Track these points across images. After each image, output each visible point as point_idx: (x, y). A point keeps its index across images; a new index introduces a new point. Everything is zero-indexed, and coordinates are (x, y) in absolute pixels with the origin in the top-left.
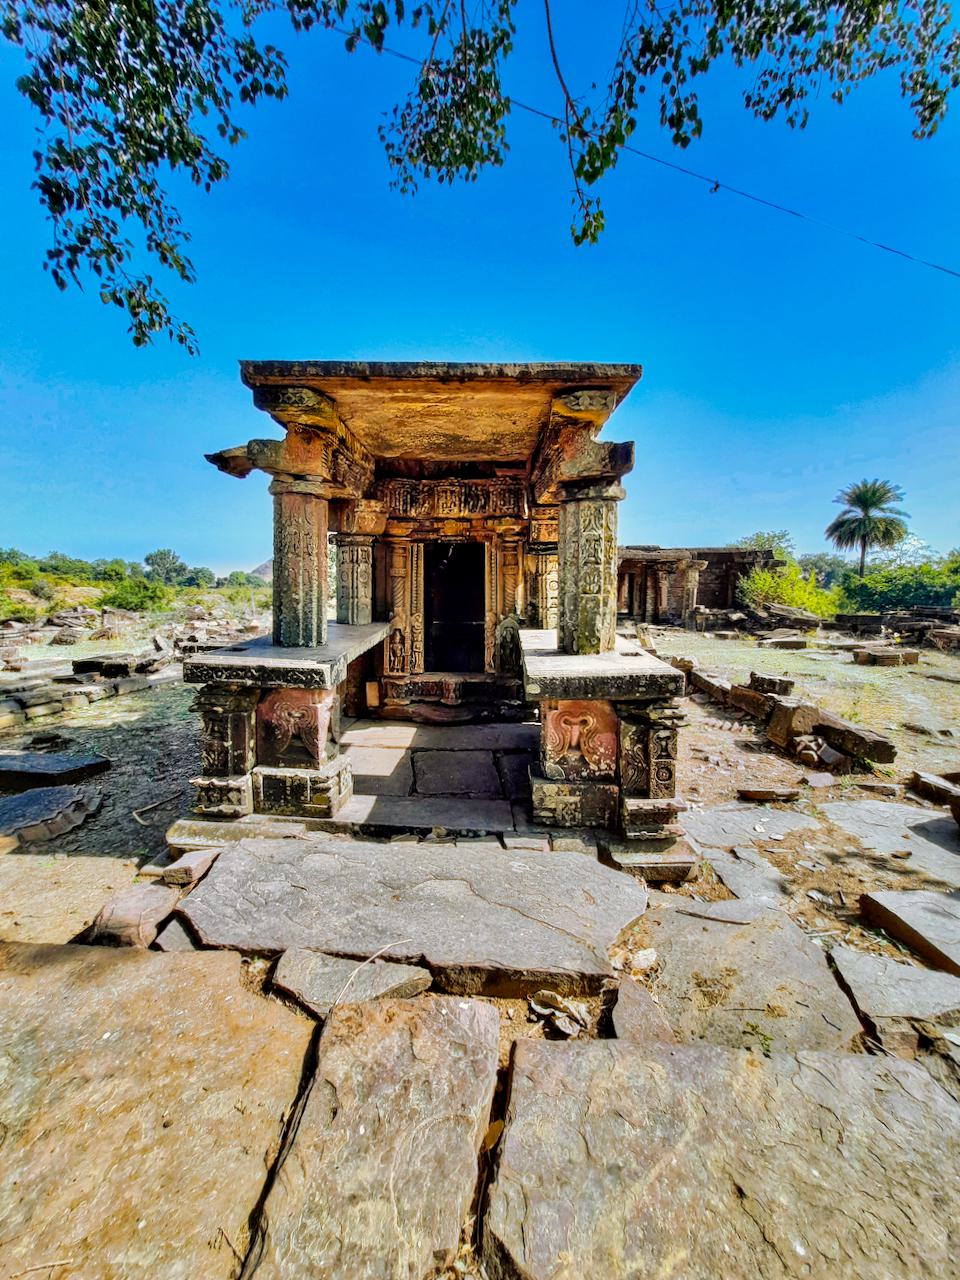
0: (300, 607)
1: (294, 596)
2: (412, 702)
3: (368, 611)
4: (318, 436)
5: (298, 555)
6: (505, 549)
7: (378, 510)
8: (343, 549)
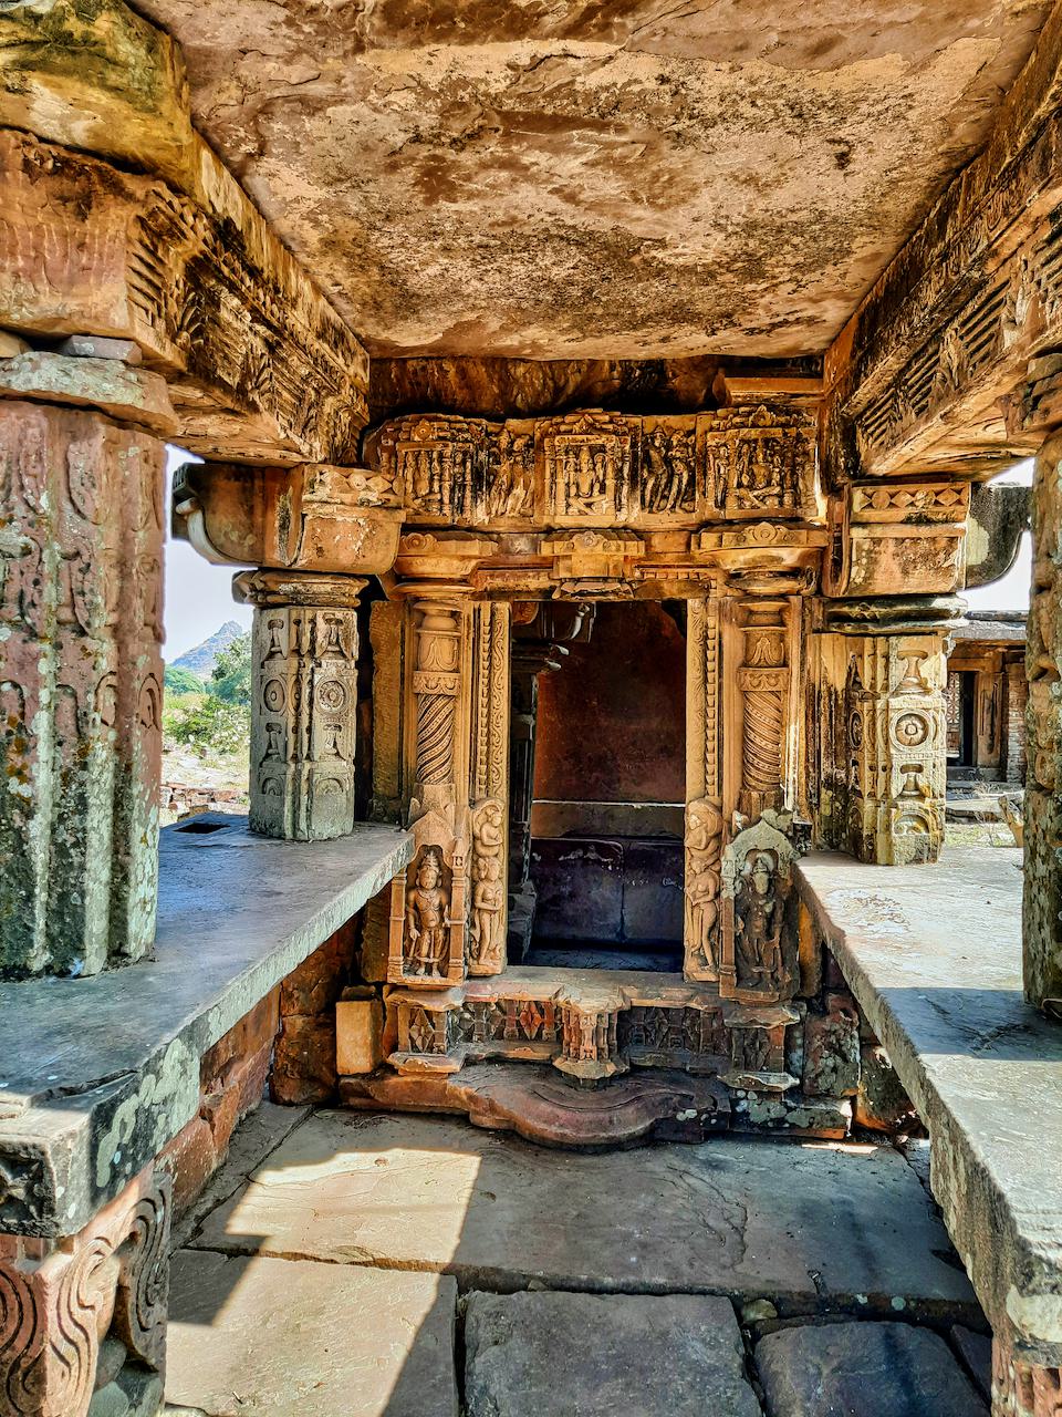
0: (38, 828)
1: (15, 786)
2: (469, 1062)
3: (344, 799)
4: (118, 190)
5: (33, 634)
6: (747, 620)
7: (374, 497)
8: (271, 615)
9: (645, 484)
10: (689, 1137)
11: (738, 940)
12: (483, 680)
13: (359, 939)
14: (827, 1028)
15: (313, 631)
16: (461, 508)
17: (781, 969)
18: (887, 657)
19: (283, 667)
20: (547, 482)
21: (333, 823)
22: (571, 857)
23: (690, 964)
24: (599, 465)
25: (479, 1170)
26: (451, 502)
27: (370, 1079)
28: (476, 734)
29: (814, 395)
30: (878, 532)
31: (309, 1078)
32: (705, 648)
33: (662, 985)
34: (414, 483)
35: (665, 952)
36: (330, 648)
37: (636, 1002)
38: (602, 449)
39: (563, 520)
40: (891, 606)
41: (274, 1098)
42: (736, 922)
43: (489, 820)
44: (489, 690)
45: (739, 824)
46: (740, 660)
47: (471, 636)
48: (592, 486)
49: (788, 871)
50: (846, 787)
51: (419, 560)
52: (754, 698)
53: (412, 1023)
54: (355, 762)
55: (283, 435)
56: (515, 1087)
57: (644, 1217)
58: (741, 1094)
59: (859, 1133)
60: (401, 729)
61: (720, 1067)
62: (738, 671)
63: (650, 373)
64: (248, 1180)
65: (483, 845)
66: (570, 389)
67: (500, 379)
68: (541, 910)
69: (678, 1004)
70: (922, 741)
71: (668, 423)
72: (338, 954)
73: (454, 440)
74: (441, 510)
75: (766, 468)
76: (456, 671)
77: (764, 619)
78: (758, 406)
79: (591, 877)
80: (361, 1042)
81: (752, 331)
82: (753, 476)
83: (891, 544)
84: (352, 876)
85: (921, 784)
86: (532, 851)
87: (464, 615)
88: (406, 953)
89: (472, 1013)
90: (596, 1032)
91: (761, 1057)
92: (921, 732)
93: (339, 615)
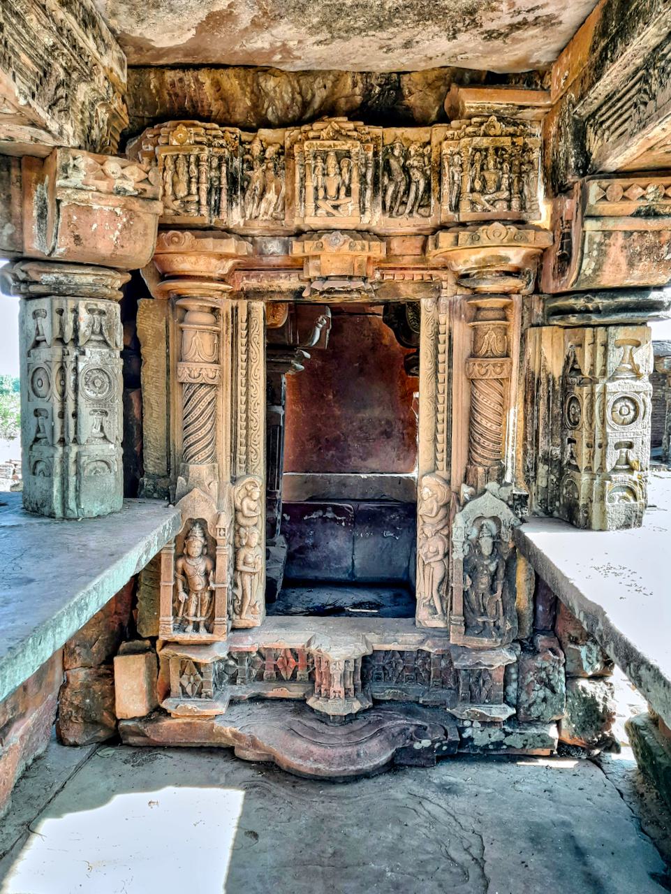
2: (233, 702)
3: (114, 480)
7: (130, 186)
9: (385, 191)
10: (423, 762)
11: (466, 594)
12: (242, 340)
13: (134, 601)
14: (539, 666)
15: (76, 321)
16: (217, 209)
17: (502, 618)
18: (605, 345)
19: (48, 354)
20: (297, 185)
21: (102, 502)
22: (314, 516)
23: (422, 613)
24: (345, 170)
25: (244, 806)
26: (209, 203)
27: (146, 722)
29: (538, 107)
30: (610, 225)
31: (91, 722)
32: (437, 341)
33: (398, 631)
34: (173, 185)
35: (397, 594)
36: (93, 337)
37: (377, 647)
38: (348, 155)
39: (313, 221)
40: (613, 298)
41: (61, 740)
42: (464, 579)
43: (248, 495)
44: (247, 440)
45: (466, 496)
46: (468, 351)
47: (230, 331)
48: (338, 190)
49: (510, 535)
50: (561, 462)
51: (179, 258)
52: (481, 385)
53: (182, 673)
54: (123, 444)
55: (22, 102)
56: (273, 724)
57: (394, 852)
58: (467, 723)
59: (564, 750)
60: (168, 415)
61: (448, 699)
62: (467, 362)
63: (389, 90)
64: (28, 829)
65: (244, 516)
66: (316, 105)
67: (252, 92)
68: (290, 557)
69: (413, 648)
70: (633, 421)
71: (406, 135)
72: (116, 613)
73: (210, 145)
74: (199, 211)
75: (496, 174)
76: (217, 362)
77: (491, 314)
78: (488, 117)
79: (328, 532)
80: (137, 690)
81: (490, 35)
82: (484, 181)
83: (621, 236)
84: (114, 556)
85: (631, 459)
87: (223, 312)
88: (175, 614)
89: (236, 661)
90: (344, 676)
91: (484, 693)
92: (632, 413)
93: (102, 305)
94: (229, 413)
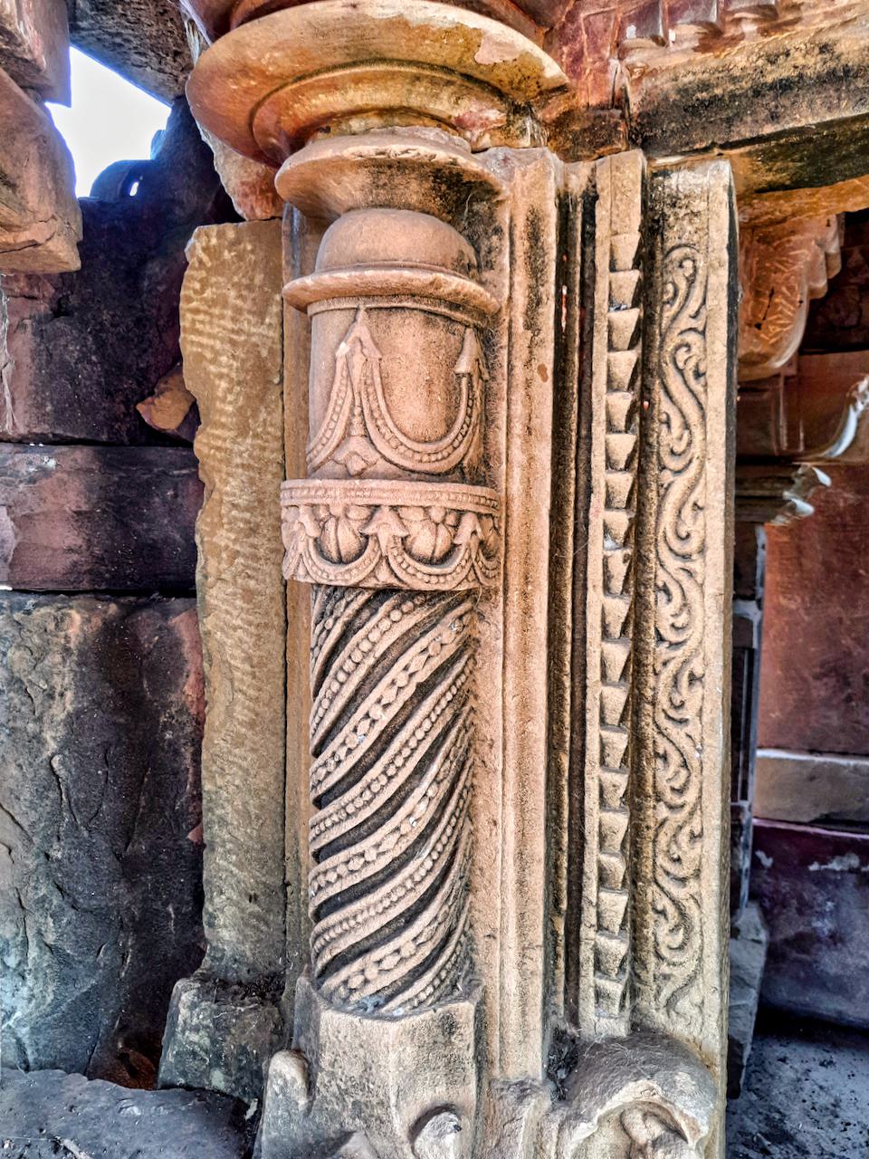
12: (608, 520)
22: (835, 865)
28: (579, 755)
44: (637, 563)
68: (775, 955)
76: (477, 472)
86: (755, 849)
87: (514, 213)
94: (539, 729)
